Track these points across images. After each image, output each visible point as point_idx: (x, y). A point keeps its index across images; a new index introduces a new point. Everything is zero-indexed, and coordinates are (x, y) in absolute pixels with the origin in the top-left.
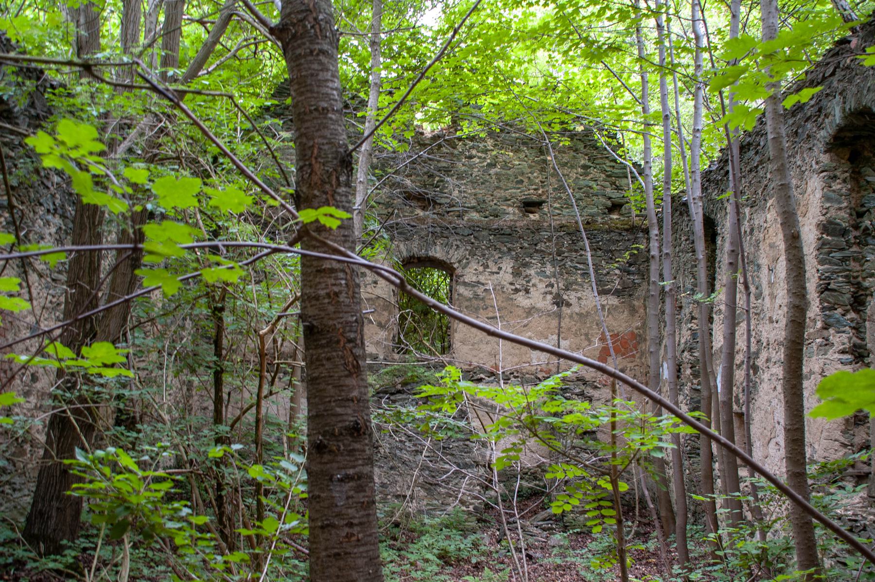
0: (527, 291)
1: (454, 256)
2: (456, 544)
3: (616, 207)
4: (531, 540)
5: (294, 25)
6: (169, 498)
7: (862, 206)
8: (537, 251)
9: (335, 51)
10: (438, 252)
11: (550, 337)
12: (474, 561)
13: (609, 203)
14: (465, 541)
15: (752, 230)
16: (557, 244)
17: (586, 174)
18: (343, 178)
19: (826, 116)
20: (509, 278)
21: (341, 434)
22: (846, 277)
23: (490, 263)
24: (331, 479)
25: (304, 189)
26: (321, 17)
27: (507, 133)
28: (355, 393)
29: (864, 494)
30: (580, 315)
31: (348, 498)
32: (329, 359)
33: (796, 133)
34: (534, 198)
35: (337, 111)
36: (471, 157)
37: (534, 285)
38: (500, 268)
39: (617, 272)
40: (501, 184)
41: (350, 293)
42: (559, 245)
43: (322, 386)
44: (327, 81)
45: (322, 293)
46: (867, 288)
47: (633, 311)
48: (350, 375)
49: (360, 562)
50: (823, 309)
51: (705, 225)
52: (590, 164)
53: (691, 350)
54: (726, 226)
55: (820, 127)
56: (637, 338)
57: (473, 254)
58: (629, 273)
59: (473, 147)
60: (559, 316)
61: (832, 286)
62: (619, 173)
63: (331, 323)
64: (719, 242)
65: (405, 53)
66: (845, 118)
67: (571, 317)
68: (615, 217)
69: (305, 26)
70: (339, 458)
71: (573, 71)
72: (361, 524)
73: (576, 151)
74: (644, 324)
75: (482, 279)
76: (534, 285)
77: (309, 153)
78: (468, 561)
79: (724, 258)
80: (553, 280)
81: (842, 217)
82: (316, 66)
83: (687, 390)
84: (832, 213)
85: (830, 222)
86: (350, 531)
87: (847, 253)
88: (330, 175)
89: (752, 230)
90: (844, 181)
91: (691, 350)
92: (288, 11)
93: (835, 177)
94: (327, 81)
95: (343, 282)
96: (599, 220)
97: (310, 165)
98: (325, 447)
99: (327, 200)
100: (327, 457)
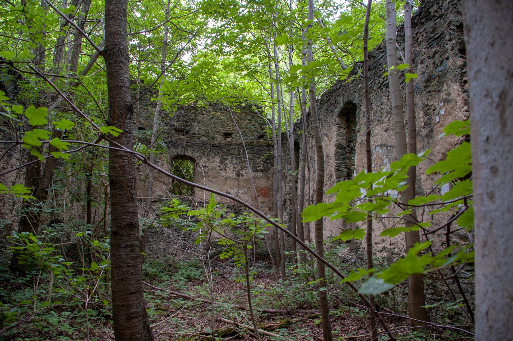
0: (226, 170)
1: (195, 155)
2: (194, 273)
3: (262, 136)
4: (225, 271)
5: (109, 50)
6: (54, 254)
7: (351, 138)
8: (230, 154)
9: (127, 62)
10: (189, 153)
11: (235, 189)
12: (201, 280)
13: (259, 135)
14: (198, 272)
15: (312, 147)
16: (238, 151)
17: (250, 123)
18: (128, 116)
19: (338, 103)
20: (218, 164)
21: (124, 227)
22: (345, 165)
23: (210, 158)
24: (120, 247)
25: (111, 120)
26: (121, 47)
27: (216, 106)
28: (131, 210)
29: (348, 248)
30: (247, 180)
31: (127, 255)
32: (119, 195)
33: (328, 109)
34: (229, 132)
35: (127, 87)
36: (203, 115)
37: (228, 168)
38: (214, 160)
39: (262, 162)
40: (216, 126)
41: (130, 166)
42: (239, 151)
43: (117, 206)
44: (123, 74)
45: (117, 165)
46: (352, 170)
47: (268, 178)
48: (129, 202)
49: (133, 282)
50: (337, 178)
51: (295, 144)
52: (250, 118)
53: (289, 194)
54: (302, 146)
55: (336, 108)
56: (270, 189)
57: (203, 154)
58: (267, 163)
59: (204, 111)
60: (238, 180)
61: (340, 169)
62: (262, 124)
63: (121, 178)
64: (300, 151)
65: (176, 71)
66: (344, 105)
67: (243, 180)
68: (261, 140)
69: (114, 51)
70: (124, 238)
71: (245, 82)
72: (133, 266)
73: (246, 113)
74: (272, 184)
75: (207, 165)
76: (228, 168)
77: (113, 105)
78: (198, 280)
79: (301, 157)
80: (236, 165)
81: (344, 142)
82: (118, 68)
83: (288, 210)
84: (340, 141)
85: (339, 144)
86: (128, 269)
87: (345, 156)
88: (122, 114)
89: (312, 147)
90: (344, 129)
91: (289, 194)
92: (107, 44)
93: (341, 127)
94: (123, 74)
95: (127, 161)
96: (255, 141)
97: (114, 110)
98: (117, 233)
99: (121, 125)
100: (118, 237)
